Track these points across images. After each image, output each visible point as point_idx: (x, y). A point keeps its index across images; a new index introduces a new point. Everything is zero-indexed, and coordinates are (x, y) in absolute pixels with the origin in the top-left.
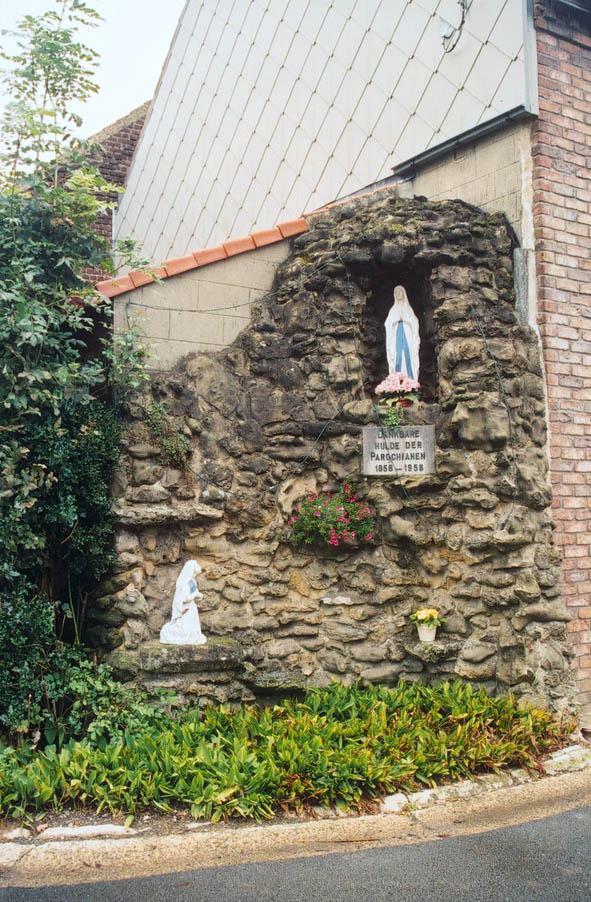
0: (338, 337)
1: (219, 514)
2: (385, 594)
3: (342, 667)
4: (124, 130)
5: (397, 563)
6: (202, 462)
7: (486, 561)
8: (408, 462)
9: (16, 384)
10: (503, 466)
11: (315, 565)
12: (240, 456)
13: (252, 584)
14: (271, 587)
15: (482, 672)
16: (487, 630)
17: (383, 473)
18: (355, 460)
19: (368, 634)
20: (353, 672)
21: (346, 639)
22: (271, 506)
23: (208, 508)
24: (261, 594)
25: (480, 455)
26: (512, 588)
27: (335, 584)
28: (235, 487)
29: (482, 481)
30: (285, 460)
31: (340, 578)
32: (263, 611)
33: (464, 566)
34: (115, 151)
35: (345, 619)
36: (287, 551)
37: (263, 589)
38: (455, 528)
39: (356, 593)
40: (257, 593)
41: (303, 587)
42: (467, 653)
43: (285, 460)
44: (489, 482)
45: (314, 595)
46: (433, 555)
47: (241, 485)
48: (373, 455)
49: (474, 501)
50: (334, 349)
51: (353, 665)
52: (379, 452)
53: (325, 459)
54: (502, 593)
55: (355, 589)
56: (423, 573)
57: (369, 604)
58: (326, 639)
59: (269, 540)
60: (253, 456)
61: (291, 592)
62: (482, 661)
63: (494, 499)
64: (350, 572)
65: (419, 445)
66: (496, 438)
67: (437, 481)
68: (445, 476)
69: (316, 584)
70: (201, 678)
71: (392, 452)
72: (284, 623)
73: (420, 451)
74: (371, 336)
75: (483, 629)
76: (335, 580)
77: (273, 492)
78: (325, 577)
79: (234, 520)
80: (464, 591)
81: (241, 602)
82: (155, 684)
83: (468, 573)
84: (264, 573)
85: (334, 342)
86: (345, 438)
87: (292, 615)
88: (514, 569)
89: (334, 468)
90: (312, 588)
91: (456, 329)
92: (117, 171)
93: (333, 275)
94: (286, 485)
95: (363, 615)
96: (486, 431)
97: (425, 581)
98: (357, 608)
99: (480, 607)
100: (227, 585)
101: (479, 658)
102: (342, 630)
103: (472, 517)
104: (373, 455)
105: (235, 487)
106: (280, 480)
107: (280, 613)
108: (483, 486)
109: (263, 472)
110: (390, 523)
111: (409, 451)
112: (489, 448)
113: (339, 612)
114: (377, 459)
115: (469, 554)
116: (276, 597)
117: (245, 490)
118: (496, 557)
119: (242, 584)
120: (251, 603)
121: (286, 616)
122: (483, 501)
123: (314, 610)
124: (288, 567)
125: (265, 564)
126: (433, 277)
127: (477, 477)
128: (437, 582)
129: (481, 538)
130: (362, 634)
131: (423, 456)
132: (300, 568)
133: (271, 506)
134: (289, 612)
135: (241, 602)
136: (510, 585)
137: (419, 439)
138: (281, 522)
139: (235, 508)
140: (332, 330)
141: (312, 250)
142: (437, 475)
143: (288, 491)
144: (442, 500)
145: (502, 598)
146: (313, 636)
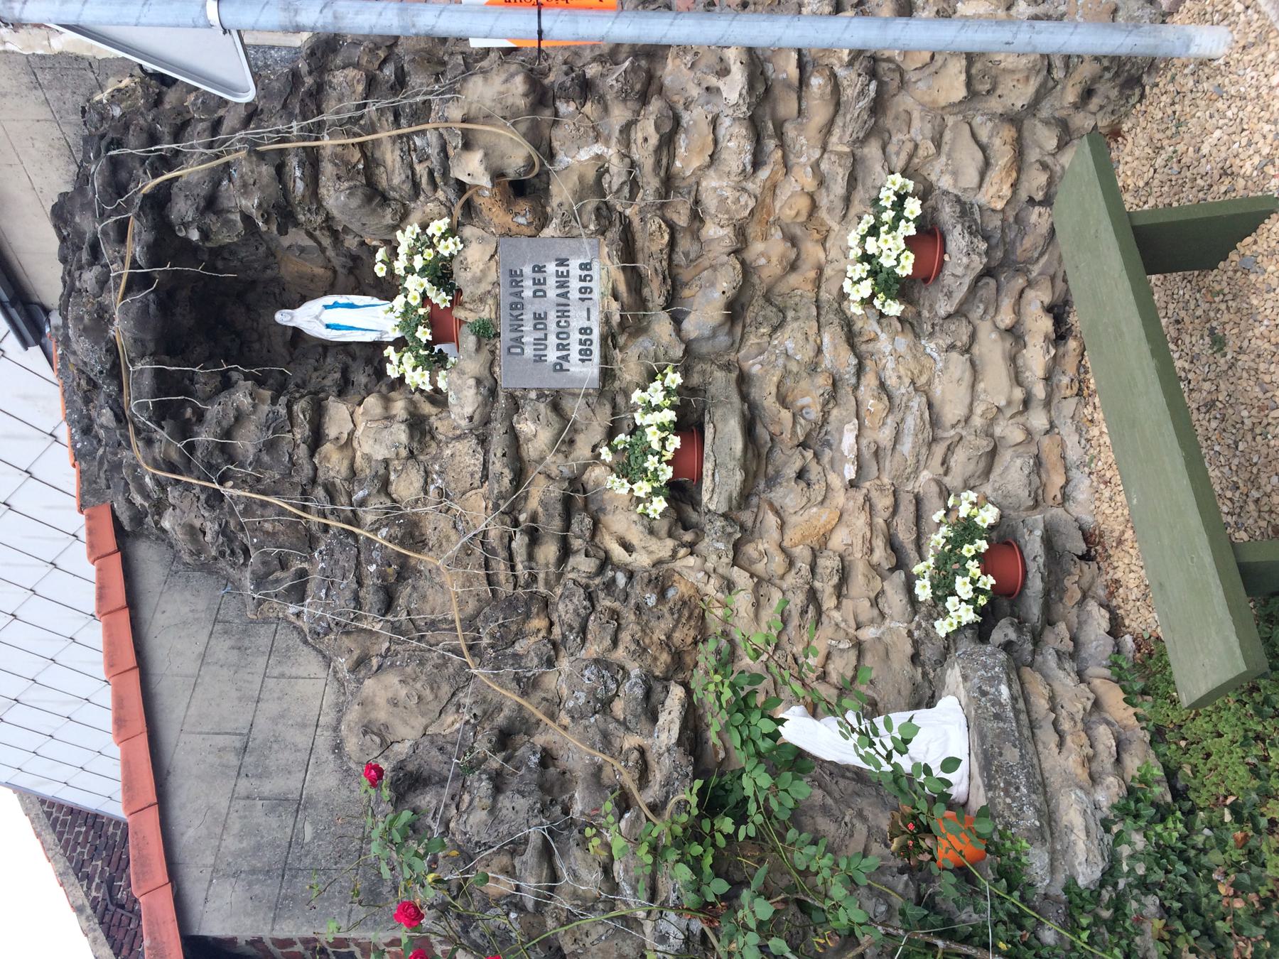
0: (316, 439)
1: (677, 692)
2: (837, 357)
3: (985, 444)
4: (54, 826)
5: (775, 329)
6: (565, 728)
7: (780, 134)
8: (574, 295)
9: (569, 712)
10: (585, 89)
11: (777, 495)
12: (555, 645)
13: (818, 622)
14: (826, 587)
15: (1008, 147)
16: (919, 138)
17: (596, 348)
18: (567, 404)
19: (916, 390)
20: (992, 422)
21: (928, 433)
22: (661, 583)
23: (663, 718)
24: (838, 607)
25: (559, 137)
26: (841, 72)
27: (816, 455)
28: (620, 654)
29: (617, 133)
30: (566, 552)
31: (804, 445)
32: (875, 602)
33: (785, 192)
34: (86, 839)
35: (885, 436)
36: (750, 550)
37: (829, 602)
38: (710, 202)
39: (835, 412)
40: (836, 615)
41: (822, 517)
42: (970, 176)
43: (566, 552)
44: (619, 114)
45: (840, 498)
46: (762, 254)
47: (615, 642)
48: (559, 368)
49: (658, 150)
50: (342, 448)
51: (977, 421)
52: (552, 355)
53: (565, 470)
54: (849, 93)
55: (825, 414)
56: (794, 279)
57: (856, 387)
58: (925, 475)
59: (729, 586)
60: (555, 618)
61: (831, 544)
62: (983, 148)
63: (655, 105)
64: (795, 422)
65: (539, 269)
66: (526, 95)
67: (614, 233)
68: (604, 214)
69: (818, 491)
70: (1053, 746)
71: (552, 327)
72: (894, 561)
73: (551, 268)
74: (328, 382)
75: (916, 146)
76: (809, 454)
77: (631, 575)
78: (801, 475)
79: (688, 660)
80: (839, 188)
81: (858, 646)
82: (1082, 857)
83: (804, 178)
84: (798, 600)
85: (327, 448)
86: (526, 427)
87: (879, 544)
88: (801, 65)
89: (582, 451)
90: (822, 502)
91: (300, 185)
92: (118, 839)
93: (133, 423)
94: (618, 552)
95: (880, 399)
96: (511, 116)
97: (812, 274)
98: (863, 413)
99: (872, 150)
100: (823, 677)
101: (979, 155)
102: (907, 446)
103: (687, 159)
104: (559, 368)
105: (620, 654)
106: (606, 562)
107: (875, 568)
108: (627, 128)
109: (590, 597)
110: (696, 339)
111: (552, 293)
112: (547, 115)
113: (873, 448)
114: (565, 358)
115: (764, 174)
116: (844, 575)
117: (625, 637)
118: (774, 110)
119: (821, 645)
120: (858, 628)
121: (880, 554)
122: (657, 128)
123: (867, 499)
124: (782, 549)
125: (777, 596)
126: (195, 235)
127: (607, 143)
128: (813, 251)
129: (736, 146)
130: (918, 402)
131: (562, 262)
132: (782, 527)
133: (661, 583)
134: (872, 550)
135: (858, 646)
136: (834, 76)
137: (527, 270)
138: (691, 561)
139: (665, 657)
140: (303, 451)
141: (146, 496)
142: (602, 232)
143: (628, 547)
144: (654, 224)
145: (862, 93)
146: (918, 501)
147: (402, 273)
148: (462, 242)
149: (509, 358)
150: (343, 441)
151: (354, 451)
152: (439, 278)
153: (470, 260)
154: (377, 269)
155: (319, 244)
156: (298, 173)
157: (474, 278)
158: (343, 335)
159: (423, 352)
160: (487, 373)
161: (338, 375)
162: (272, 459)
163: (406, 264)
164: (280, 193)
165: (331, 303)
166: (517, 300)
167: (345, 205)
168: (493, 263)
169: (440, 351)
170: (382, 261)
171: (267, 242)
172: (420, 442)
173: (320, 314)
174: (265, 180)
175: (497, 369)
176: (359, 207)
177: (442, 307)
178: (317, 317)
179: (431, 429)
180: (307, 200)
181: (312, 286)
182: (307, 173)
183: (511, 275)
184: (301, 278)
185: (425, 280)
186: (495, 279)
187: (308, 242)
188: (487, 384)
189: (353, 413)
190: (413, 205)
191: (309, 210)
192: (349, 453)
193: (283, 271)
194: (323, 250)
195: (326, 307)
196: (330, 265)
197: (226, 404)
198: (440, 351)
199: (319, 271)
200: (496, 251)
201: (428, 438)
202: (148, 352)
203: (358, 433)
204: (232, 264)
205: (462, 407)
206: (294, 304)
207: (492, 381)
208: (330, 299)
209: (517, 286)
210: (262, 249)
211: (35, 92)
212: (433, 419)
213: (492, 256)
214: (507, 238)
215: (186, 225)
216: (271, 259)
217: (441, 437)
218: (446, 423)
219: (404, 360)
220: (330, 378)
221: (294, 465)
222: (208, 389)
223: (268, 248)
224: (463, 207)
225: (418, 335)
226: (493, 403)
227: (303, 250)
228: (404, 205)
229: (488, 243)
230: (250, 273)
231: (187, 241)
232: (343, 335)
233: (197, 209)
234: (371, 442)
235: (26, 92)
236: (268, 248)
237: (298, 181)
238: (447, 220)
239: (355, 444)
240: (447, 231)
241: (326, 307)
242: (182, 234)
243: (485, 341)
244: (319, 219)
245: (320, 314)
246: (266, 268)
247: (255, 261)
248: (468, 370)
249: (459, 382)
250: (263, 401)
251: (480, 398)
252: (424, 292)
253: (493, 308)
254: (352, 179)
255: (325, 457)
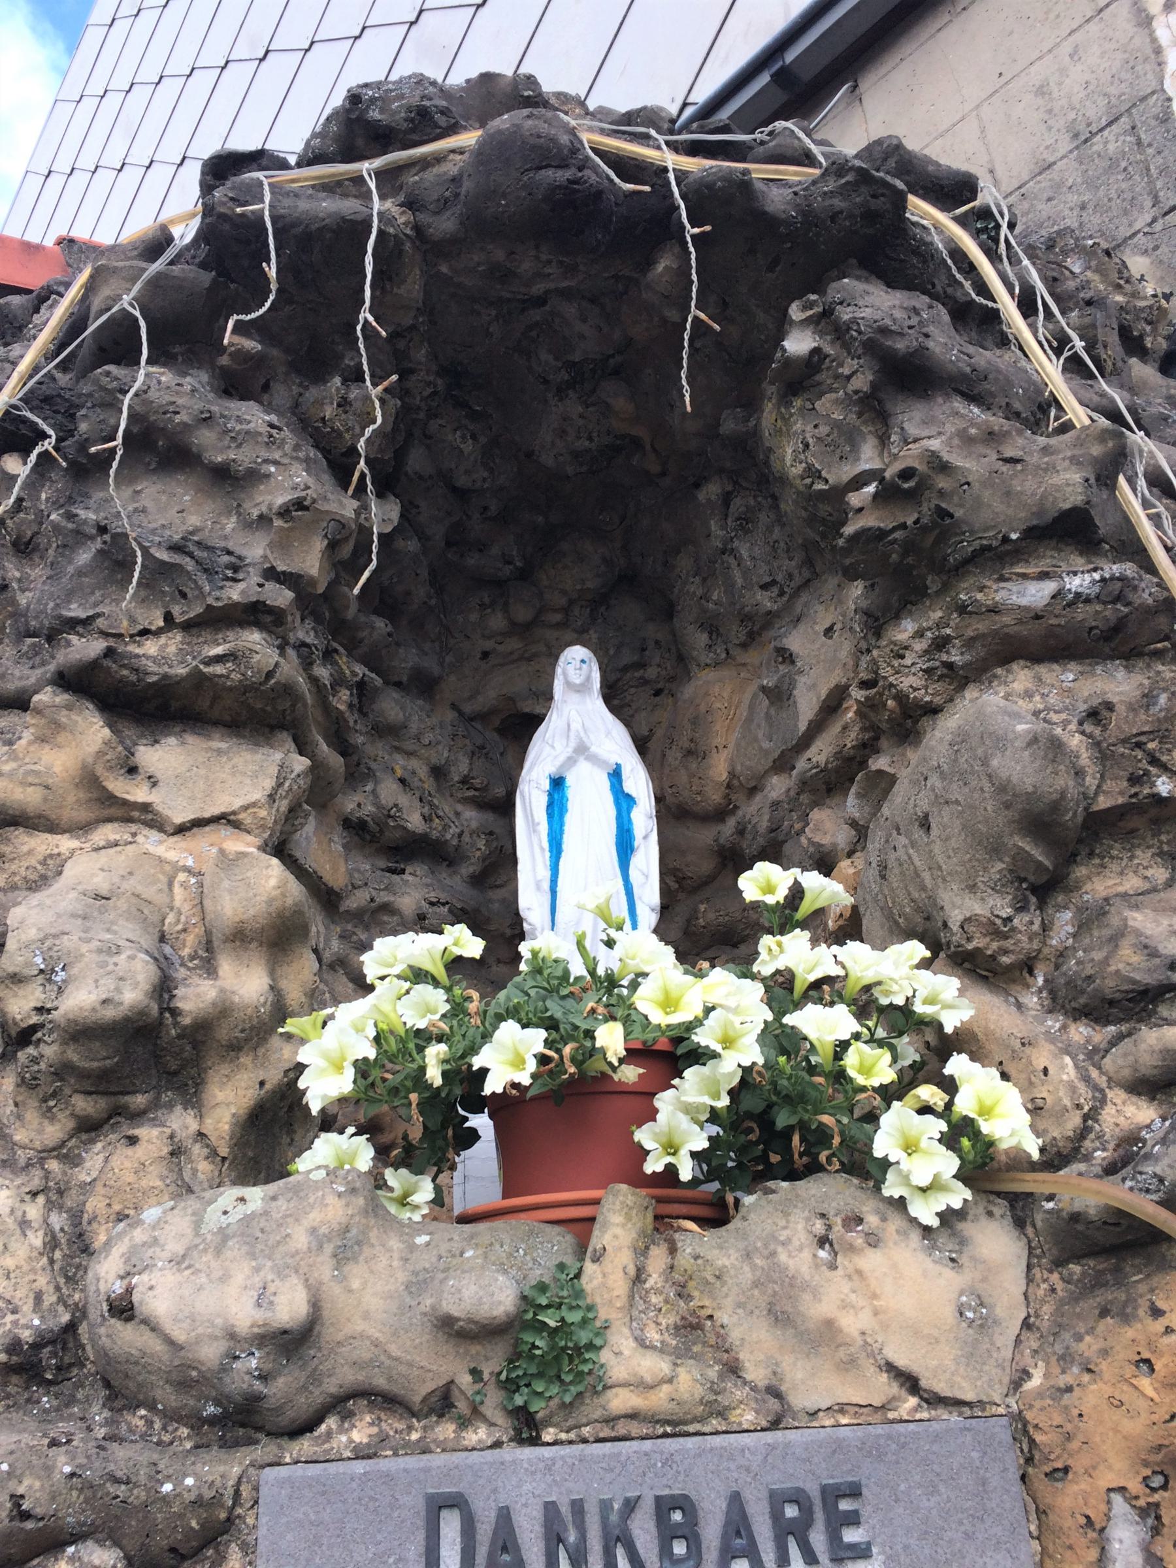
50: (90, 781)
126: (798, 344)
147: (765, 966)
148: (948, 1217)
149: (413, 1504)
150: (119, 786)
151: (81, 828)
152: (765, 1119)
153: (871, 1261)
154: (764, 869)
155: (805, 741)
156: (1077, 583)
157: (792, 1285)
158: (533, 826)
159: (434, 1060)
160: (342, 1377)
161: (414, 821)
162: (80, 573)
163: (806, 975)
164: (989, 537)
165: (629, 787)
166: (711, 1532)
167: (1000, 742)
168: (881, 1388)
169: (473, 1136)
170: (797, 893)
171: (788, 606)
172: (62, 1071)
173: (594, 759)
174: (1028, 486)
175: (360, 1433)
176: (1002, 788)
177: (644, 1136)
178: (582, 750)
179: (137, 1116)
180: (980, 626)
181: (674, 757)
182: (1082, 612)
183: (832, 1494)
184: (695, 722)
185: (751, 1053)
186: (801, 1400)
187: (807, 705)
188: (277, 1389)
189: (236, 825)
190: (1031, 1000)
191: (941, 644)
192: (72, 807)
193: (708, 675)
194: (783, 764)
195: (616, 775)
196: (738, 797)
197: (271, 442)
198: (473, 1136)
199: (719, 768)
200: (934, 1400)
201: (84, 1105)
202: (423, 218)
203: (151, 842)
204: (714, 526)
205: (179, 1262)
206: (613, 696)
207: (303, 1405)
208: (638, 782)
209: (784, 1531)
210: (766, 601)
211: (1067, 137)
212: (182, 1121)
213: (910, 1382)
214: (1012, 1461)
215: (824, 320)
216: (737, 633)
217: (94, 1160)
218: (153, 1179)
219: (425, 991)
220: (404, 800)
221: (50, 639)
222: (329, 411)
223: (770, 618)
224: (1119, 1218)
225: (509, 1030)
226: (197, 1422)
227: (780, 696)
228: (1028, 966)
229: (972, 1356)
230: (695, 587)
231: (782, 325)
232: (533, 826)
233: (884, 331)
234: (101, 883)
235: (1060, 123)
236: (770, 618)
237: (1050, 587)
238: (1032, 1147)
239: (110, 832)
240: (986, 1145)
241: (616, 775)
242: (795, 312)
243: (493, 1362)
244: (911, 682)
245: (594, 759)
246: (713, 629)
247: (730, 586)
248: (357, 1274)
249: (300, 1239)
250: (282, 544)
251: (210, 1353)
252: (699, 1056)
253: (658, 1400)
254: (1103, 754)
255: (58, 726)
